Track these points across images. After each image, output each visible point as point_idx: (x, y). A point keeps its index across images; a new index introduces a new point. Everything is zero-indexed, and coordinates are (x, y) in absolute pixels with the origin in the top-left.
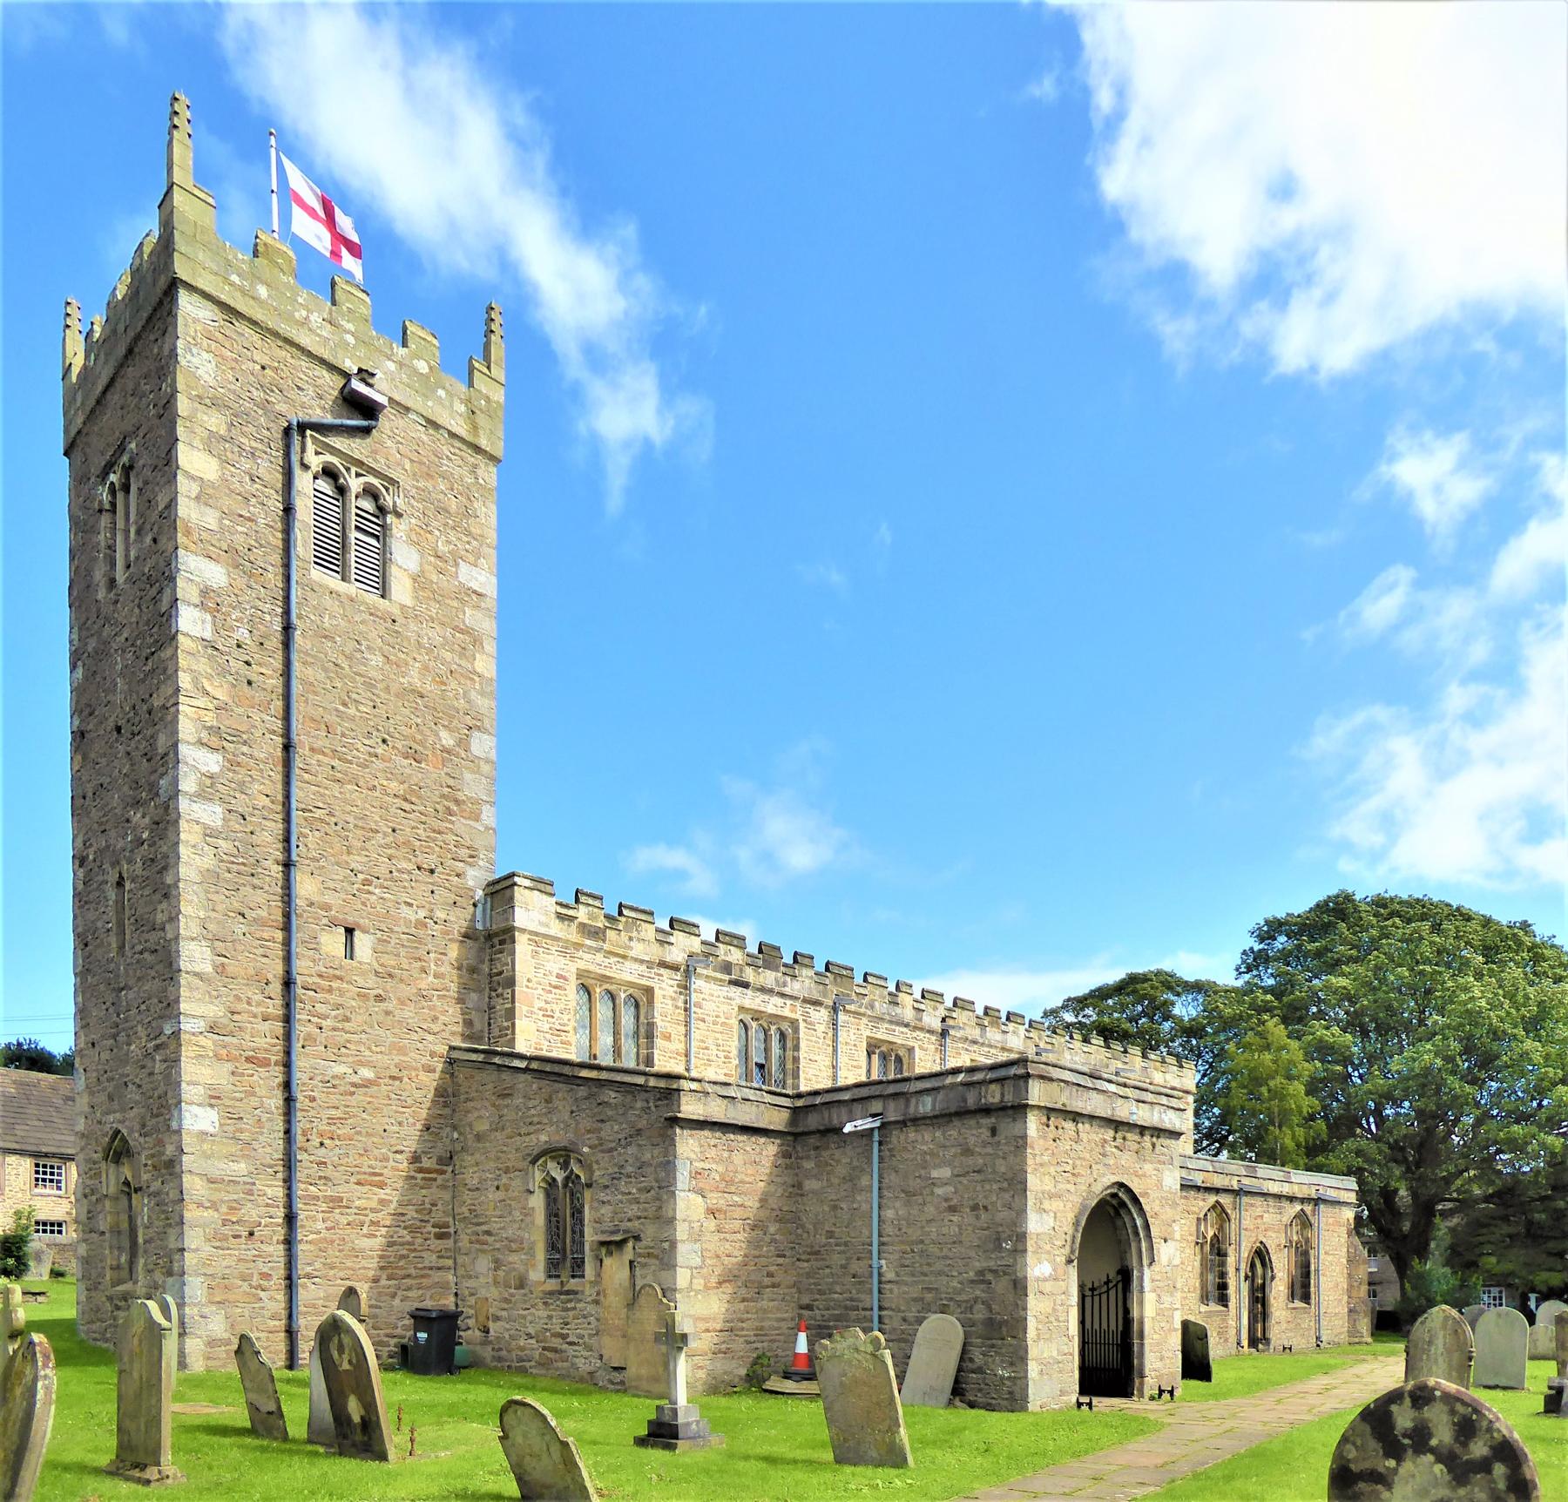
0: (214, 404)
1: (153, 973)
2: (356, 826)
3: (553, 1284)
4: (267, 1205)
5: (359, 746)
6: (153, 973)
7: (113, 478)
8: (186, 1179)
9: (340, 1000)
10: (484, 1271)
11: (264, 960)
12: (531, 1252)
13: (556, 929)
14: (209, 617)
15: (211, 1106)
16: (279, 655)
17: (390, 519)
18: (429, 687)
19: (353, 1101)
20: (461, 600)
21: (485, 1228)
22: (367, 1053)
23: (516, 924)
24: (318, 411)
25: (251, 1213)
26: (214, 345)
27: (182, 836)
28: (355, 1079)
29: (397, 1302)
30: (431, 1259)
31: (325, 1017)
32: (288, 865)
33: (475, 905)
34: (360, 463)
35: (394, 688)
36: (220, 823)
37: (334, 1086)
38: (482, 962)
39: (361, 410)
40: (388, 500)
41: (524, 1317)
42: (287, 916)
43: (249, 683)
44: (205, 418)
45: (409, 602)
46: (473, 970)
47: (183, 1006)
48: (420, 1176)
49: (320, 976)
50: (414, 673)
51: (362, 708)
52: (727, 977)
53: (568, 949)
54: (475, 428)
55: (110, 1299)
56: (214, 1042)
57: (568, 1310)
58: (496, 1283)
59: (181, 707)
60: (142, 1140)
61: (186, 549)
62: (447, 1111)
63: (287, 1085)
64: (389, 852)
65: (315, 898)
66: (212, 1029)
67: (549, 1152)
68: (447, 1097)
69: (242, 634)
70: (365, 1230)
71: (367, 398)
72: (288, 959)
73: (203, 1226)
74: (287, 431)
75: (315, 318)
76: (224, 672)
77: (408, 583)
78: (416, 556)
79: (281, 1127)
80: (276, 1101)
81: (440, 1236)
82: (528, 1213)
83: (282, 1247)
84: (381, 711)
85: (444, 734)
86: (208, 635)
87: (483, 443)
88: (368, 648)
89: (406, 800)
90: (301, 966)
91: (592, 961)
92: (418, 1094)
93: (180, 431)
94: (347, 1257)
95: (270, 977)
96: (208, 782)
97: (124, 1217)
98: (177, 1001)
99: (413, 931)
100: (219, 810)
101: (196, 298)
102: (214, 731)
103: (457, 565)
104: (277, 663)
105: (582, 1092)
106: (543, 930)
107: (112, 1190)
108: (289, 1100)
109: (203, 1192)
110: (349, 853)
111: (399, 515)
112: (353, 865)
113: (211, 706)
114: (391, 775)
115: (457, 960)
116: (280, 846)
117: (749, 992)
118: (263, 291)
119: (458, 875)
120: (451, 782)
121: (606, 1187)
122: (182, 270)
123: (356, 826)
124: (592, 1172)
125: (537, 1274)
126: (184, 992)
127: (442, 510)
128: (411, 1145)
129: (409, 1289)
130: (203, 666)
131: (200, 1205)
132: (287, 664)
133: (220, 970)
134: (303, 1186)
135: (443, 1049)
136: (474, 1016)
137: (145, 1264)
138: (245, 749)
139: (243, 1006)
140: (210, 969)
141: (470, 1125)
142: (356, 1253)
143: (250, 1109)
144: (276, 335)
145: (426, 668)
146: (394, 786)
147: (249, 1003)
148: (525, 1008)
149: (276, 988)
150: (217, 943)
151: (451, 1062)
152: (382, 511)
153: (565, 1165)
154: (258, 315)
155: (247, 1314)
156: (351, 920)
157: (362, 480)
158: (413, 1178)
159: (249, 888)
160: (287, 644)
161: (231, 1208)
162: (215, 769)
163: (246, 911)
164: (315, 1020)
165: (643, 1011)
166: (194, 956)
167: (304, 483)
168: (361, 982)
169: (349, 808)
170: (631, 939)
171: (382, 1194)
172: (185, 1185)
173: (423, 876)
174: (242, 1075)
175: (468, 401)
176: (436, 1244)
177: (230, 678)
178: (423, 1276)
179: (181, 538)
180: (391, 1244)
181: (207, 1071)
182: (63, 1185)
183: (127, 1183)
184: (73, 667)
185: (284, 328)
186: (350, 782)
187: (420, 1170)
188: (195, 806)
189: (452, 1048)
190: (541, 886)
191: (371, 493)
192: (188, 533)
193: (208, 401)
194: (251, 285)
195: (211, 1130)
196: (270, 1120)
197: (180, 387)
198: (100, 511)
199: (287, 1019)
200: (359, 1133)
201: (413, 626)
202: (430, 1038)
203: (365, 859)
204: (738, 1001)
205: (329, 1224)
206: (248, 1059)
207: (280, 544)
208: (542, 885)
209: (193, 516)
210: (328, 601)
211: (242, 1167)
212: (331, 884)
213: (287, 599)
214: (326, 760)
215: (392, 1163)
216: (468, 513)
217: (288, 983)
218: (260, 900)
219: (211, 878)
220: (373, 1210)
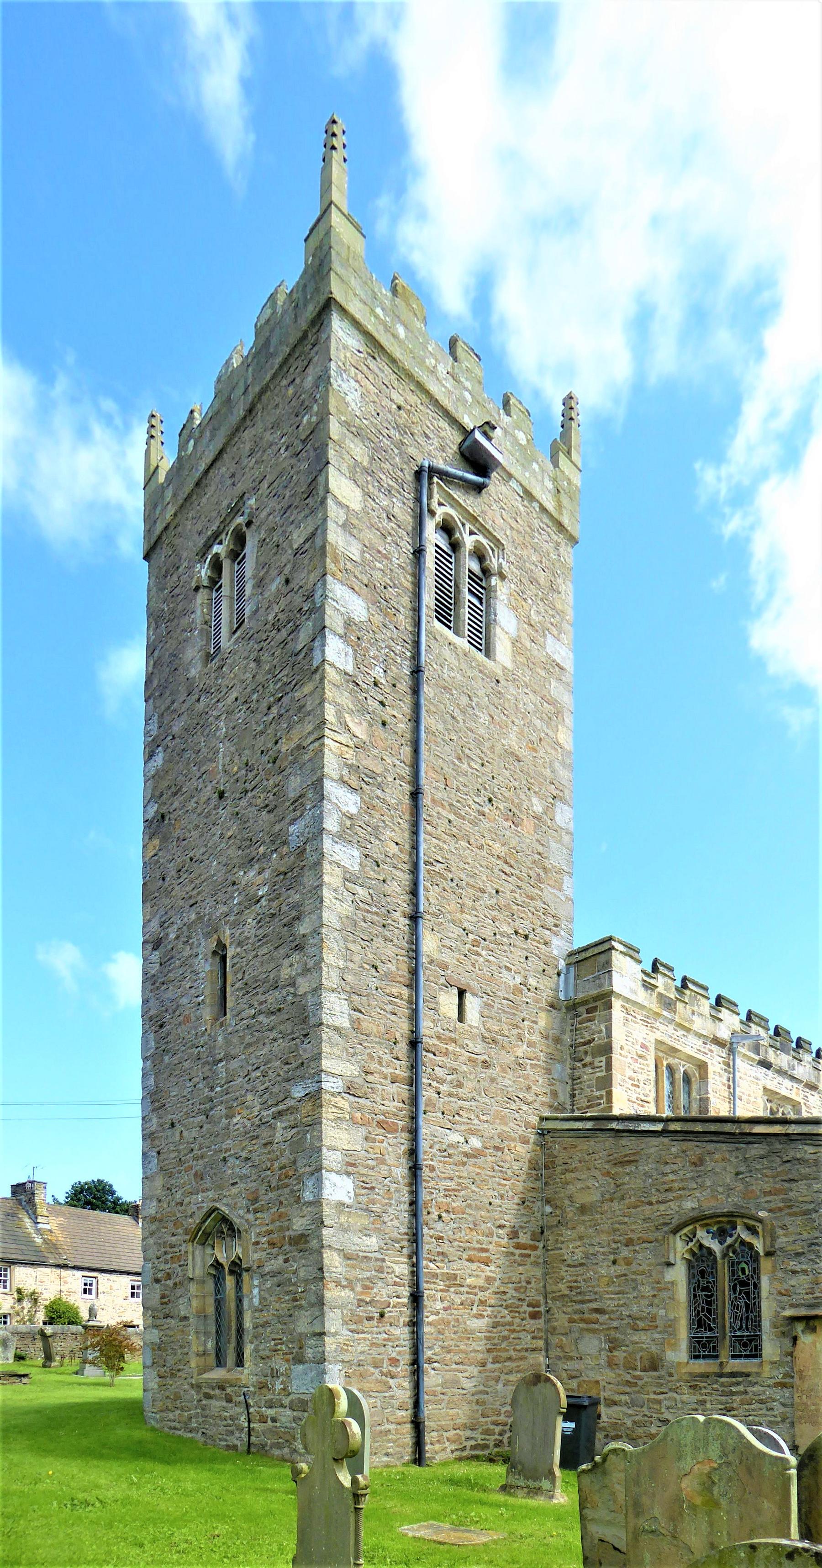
0: (358, 434)
1: (273, 1034)
2: (468, 884)
3: (701, 1366)
4: (395, 1284)
5: (471, 802)
6: (273, 1034)
7: (216, 549)
8: (327, 1254)
9: (455, 1065)
10: (594, 1351)
11: (393, 1018)
12: (670, 1327)
13: (642, 996)
14: (351, 651)
15: (348, 1174)
16: (408, 699)
17: (494, 581)
18: (523, 753)
19: (464, 1172)
20: (549, 672)
21: (594, 1305)
22: (476, 1121)
23: (616, 989)
24: (441, 462)
25: (382, 1292)
26: (360, 376)
27: (326, 878)
28: (466, 1148)
29: (500, 1387)
30: (527, 1340)
31: (441, 1081)
32: (414, 918)
33: (559, 974)
34: (474, 519)
35: (498, 749)
36: (357, 868)
37: (450, 1155)
38: (563, 1032)
39: (478, 462)
40: (493, 563)
41: (659, 1402)
42: (414, 972)
43: (384, 724)
44: (352, 446)
45: (509, 665)
46: (557, 1040)
47: (326, 1064)
48: (518, 1252)
49: (439, 1038)
50: (513, 736)
51: (472, 764)
52: (757, 1058)
53: (650, 1018)
54: (560, 506)
55: (198, 1387)
56: (351, 1104)
57: (732, 1393)
58: (611, 1364)
59: (327, 741)
60: (250, 1217)
61: (333, 575)
62: (538, 1184)
63: (413, 1153)
64: (493, 913)
65: (436, 955)
66: (350, 1090)
67: (701, 1219)
68: (545, 1170)
69: (377, 672)
70: (475, 1311)
71: (486, 451)
72: (414, 1017)
73: (341, 1307)
74: (418, 474)
75: (442, 370)
76: (363, 710)
77: (509, 645)
78: (514, 621)
79: (406, 1198)
80: (401, 1171)
81: (535, 1316)
82: (663, 1288)
83: (407, 1329)
84: (488, 769)
85: (535, 800)
86: (350, 668)
87: (566, 522)
88: (478, 704)
89: (506, 862)
90: (426, 1026)
91: (666, 1033)
92: (516, 1166)
93: (331, 453)
94: (461, 1339)
95: (398, 1035)
96: (348, 823)
97: (210, 1301)
98: (318, 1057)
99: (511, 997)
100: (356, 853)
101: (346, 324)
102: (354, 769)
103: (545, 636)
104: (406, 707)
105: (756, 1150)
106: (632, 997)
107: (198, 1272)
108: (415, 1170)
109: (340, 1269)
110: (462, 912)
111: (502, 577)
112: (466, 925)
113: (351, 744)
114: (496, 836)
115: (546, 1029)
116: (407, 897)
117: (769, 1073)
118: (401, 331)
119: (546, 944)
120: (540, 849)
121: (798, 1255)
122: (337, 291)
123: (468, 884)
124: (774, 1238)
125: (678, 1353)
126: (326, 1048)
127: (533, 581)
128: (509, 1220)
129: (510, 1373)
130: (345, 699)
131: (338, 1284)
132: (416, 707)
133: (356, 1025)
134: (425, 1262)
135: (535, 1120)
136: (559, 1087)
137: (256, 1350)
138: (379, 792)
139: (374, 1066)
140: (347, 1024)
141: (570, 1197)
142: (468, 1334)
143: (381, 1179)
144: (410, 376)
145: (521, 733)
146: (497, 847)
147: (380, 1063)
148: (619, 1076)
149: (402, 1048)
150: (355, 998)
151: (542, 1133)
152: (486, 572)
153: (721, 1235)
154: (397, 353)
155: (379, 1405)
156: (463, 982)
157: (474, 537)
158: (513, 1254)
159: (380, 940)
160: (416, 690)
161: (366, 1287)
162: (354, 810)
163: (378, 964)
164: (434, 1084)
165: (695, 1087)
166: (335, 1010)
167: (430, 526)
168: (471, 1047)
169: (462, 865)
170: (693, 1013)
171: (489, 1271)
172: (326, 1262)
173: (519, 941)
174: (374, 1141)
175: (554, 480)
176: (531, 1324)
177: (368, 716)
178: (522, 1358)
179: (330, 565)
180: (495, 1325)
181: (344, 1135)
182: (8, 1284)
183: (217, 1265)
184: (150, 756)
185: (417, 371)
186: (463, 838)
187: (518, 1246)
188: (337, 847)
189: (542, 1119)
190: (631, 952)
191: (480, 555)
192: (336, 561)
193: (354, 429)
194: (392, 321)
195: (347, 1201)
196: (397, 1190)
197: (332, 410)
198: (197, 589)
199: (413, 1082)
200: (469, 1206)
201: (512, 690)
202: (525, 1107)
203: (475, 919)
204: (762, 1083)
205: (446, 1304)
206: (380, 1124)
207: (409, 585)
208: (632, 952)
209: (340, 543)
210: (447, 653)
211: (373, 1242)
212: (447, 942)
213: (417, 644)
214: (444, 813)
215: (495, 1239)
216: (553, 588)
217: (414, 1044)
218: (389, 953)
219: (350, 927)
220: (483, 1289)
